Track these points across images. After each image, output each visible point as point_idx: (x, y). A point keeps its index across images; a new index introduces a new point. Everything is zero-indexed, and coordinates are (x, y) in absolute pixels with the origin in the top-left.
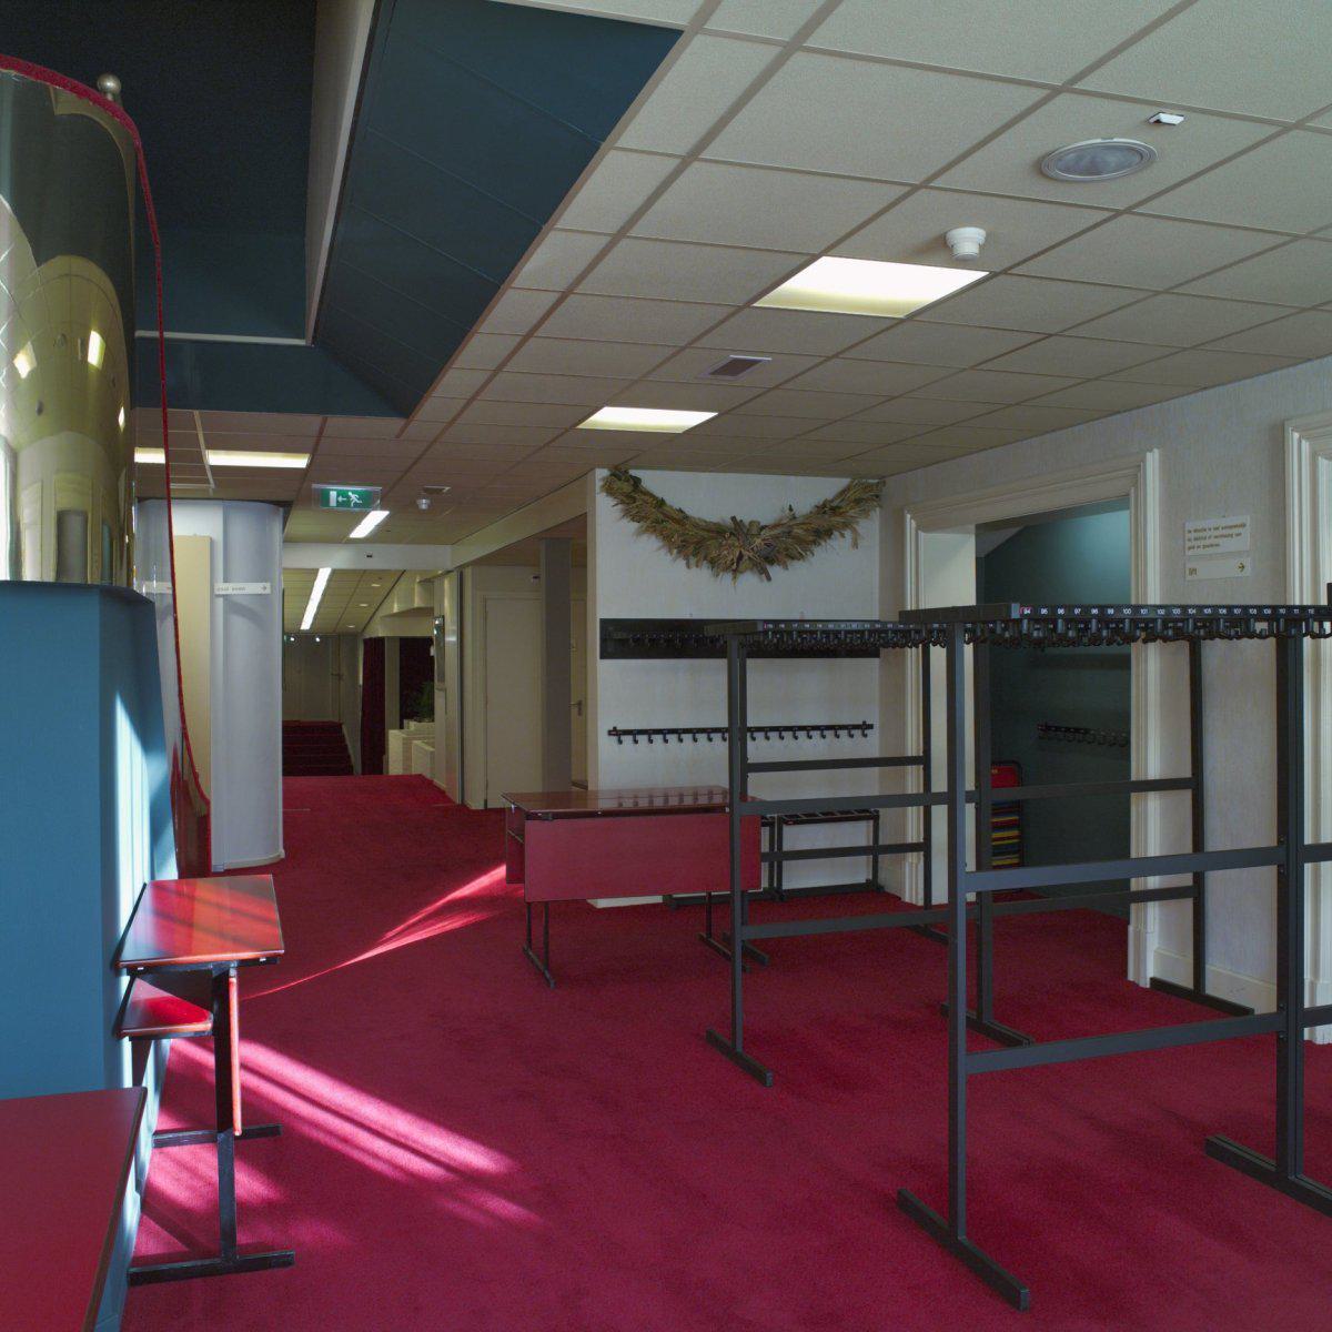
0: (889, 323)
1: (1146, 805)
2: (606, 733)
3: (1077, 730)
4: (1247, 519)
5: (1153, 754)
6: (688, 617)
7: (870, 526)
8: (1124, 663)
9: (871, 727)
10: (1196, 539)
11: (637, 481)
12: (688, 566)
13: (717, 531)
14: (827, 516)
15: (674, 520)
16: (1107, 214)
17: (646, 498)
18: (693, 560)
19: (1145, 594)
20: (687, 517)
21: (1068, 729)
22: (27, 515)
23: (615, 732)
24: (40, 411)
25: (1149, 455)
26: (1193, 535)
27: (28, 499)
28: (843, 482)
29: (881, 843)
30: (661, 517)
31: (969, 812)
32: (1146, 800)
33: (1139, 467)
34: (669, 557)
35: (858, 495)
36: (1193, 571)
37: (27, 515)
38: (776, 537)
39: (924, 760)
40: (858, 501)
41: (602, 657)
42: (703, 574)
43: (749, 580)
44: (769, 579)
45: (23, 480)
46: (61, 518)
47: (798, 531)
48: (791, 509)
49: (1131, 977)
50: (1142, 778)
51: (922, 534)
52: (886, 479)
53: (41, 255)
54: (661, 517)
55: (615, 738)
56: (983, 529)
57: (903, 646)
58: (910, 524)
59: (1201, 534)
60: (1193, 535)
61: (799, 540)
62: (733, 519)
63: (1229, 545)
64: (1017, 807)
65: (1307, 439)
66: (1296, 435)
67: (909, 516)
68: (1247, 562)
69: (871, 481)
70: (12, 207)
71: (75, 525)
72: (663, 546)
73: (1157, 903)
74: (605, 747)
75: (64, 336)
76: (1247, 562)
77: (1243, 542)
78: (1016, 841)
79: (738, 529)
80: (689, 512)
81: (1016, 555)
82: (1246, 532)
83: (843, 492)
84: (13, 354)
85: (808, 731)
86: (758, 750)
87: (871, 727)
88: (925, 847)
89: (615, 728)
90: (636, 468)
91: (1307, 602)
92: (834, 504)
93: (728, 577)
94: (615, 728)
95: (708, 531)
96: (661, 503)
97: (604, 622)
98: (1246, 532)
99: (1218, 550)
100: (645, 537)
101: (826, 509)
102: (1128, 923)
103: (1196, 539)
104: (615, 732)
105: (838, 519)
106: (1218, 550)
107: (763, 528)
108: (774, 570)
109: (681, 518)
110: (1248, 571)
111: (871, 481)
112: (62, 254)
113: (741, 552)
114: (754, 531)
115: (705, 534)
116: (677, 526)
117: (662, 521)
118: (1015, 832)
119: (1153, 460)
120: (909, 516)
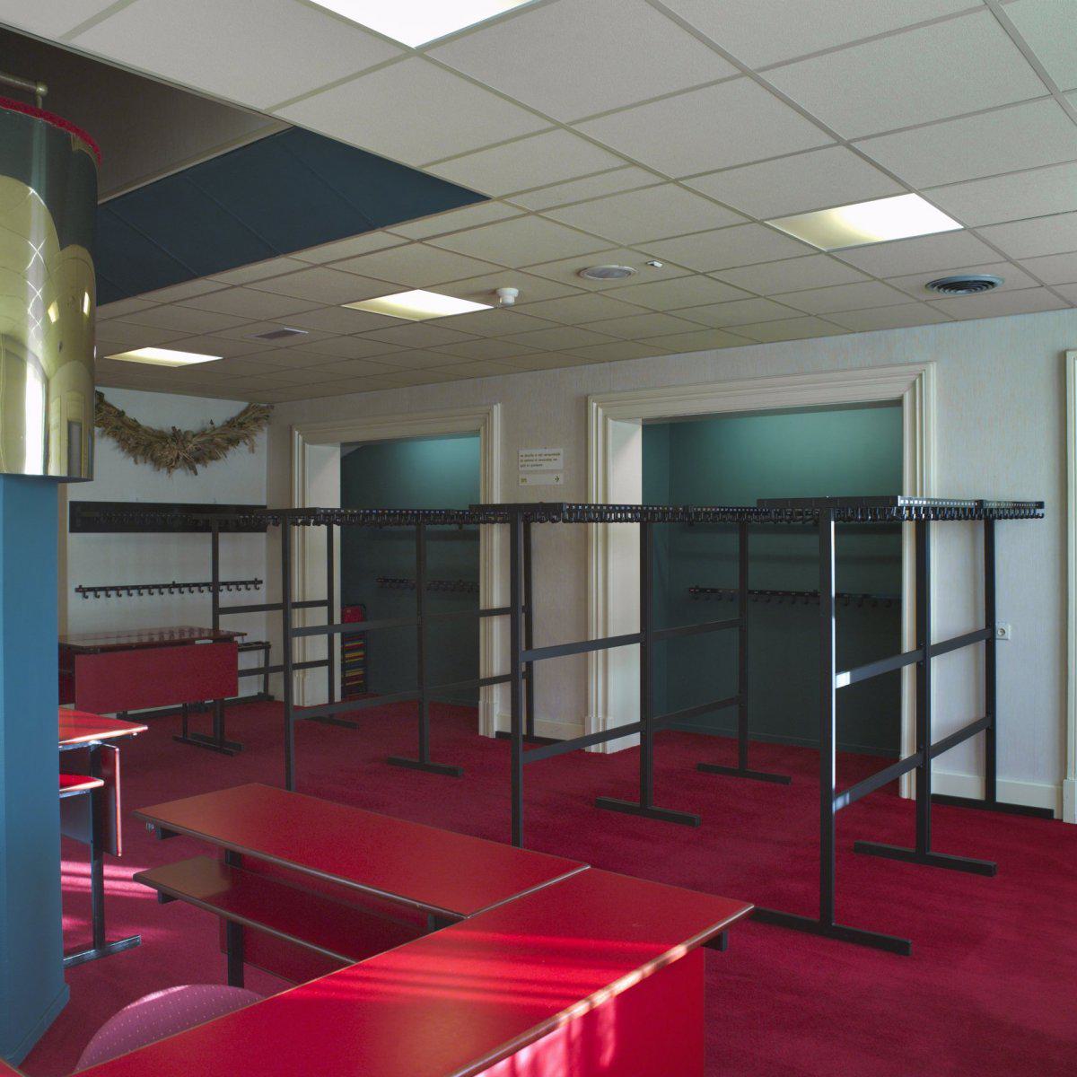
0: (402, 322)
1: (492, 624)
2: (74, 591)
3: (401, 581)
4: (561, 451)
5: (495, 591)
6: (135, 501)
7: (262, 438)
8: (476, 536)
9: (261, 582)
10: (526, 461)
11: (101, 396)
12: (136, 462)
13: (161, 437)
14: (236, 430)
15: (130, 427)
16: (407, 241)
17: (111, 409)
18: (139, 458)
19: (492, 497)
20: (139, 426)
21: (394, 581)
22: (54, 420)
23: (80, 590)
24: (61, 348)
25: (495, 407)
26: (524, 458)
27: (54, 407)
28: (243, 405)
29: (270, 665)
30: (120, 424)
31: (337, 637)
32: (492, 621)
33: (489, 414)
34: (122, 455)
35: (256, 415)
36: (524, 480)
37: (54, 420)
38: (203, 443)
39: (329, 603)
40: (256, 420)
41: (73, 530)
42: (145, 469)
43: (180, 474)
44: (196, 474)
45: (52, 397)
46: (70, 424)
47: (218, 439)
48: (212, 423)
49: (481, 733)
50: (490, 608)
51: (307, 446)
52: (275, 405)
53: (63, 244)
54: (120, 424)
55: (80, 594)
56: (343, 445)
57: (493, 522)
58: (298, 438)
59: (531, 458)
60: (524, 458)
61: (218, 446)
62: (174, 428)
63: (546, 465)
64: (361, 635)
65: (601, 407)
66: (595, 404)
67: (297, 433)
68: (561, 476)
69: (262, 405)
70: (46, 203)
71: (75, 429)
72: (119, 447)
73: (498, 685)
74: (74, 600)
75: (73, 298)
76: (561, 476)
77: (559, 464)
78: (361, 659)
79: (177, 436)
80: (141, 422)
81: (362, 465)
82: (560, 458)
83: (245, 412)
84: (47, 307)
85: (160, 589)
86: (226, 598)
87: (261, 582)
88: (329, 663)
89: (80, 586)
90: (101, 385)
91: (600, 502)
92: (241, 420)
93: (164, 471)
94: (80, 586)
95: (156, 437)
96: (121, 414)
97: (73, 504)
98: (560, 458)
99: (541, 468)
100: (105, 439)
101: (231, 424)
102: (479, 700)
103: (526, 461)
104: (80, 590)
105: (243, 431)
106: (541, 468)
107: (194, 436)
108: (199, 467)
109: (135, 426)
110: (561, 481)
111: (262, 405)
112: (73, 243)
113: (178, 454)
114: (189, 437)
115: (153, 439)
116: (131, 432)
117: (121, 427)
118: (360, 653)
119: (497, 410)
120: (297, 433)
